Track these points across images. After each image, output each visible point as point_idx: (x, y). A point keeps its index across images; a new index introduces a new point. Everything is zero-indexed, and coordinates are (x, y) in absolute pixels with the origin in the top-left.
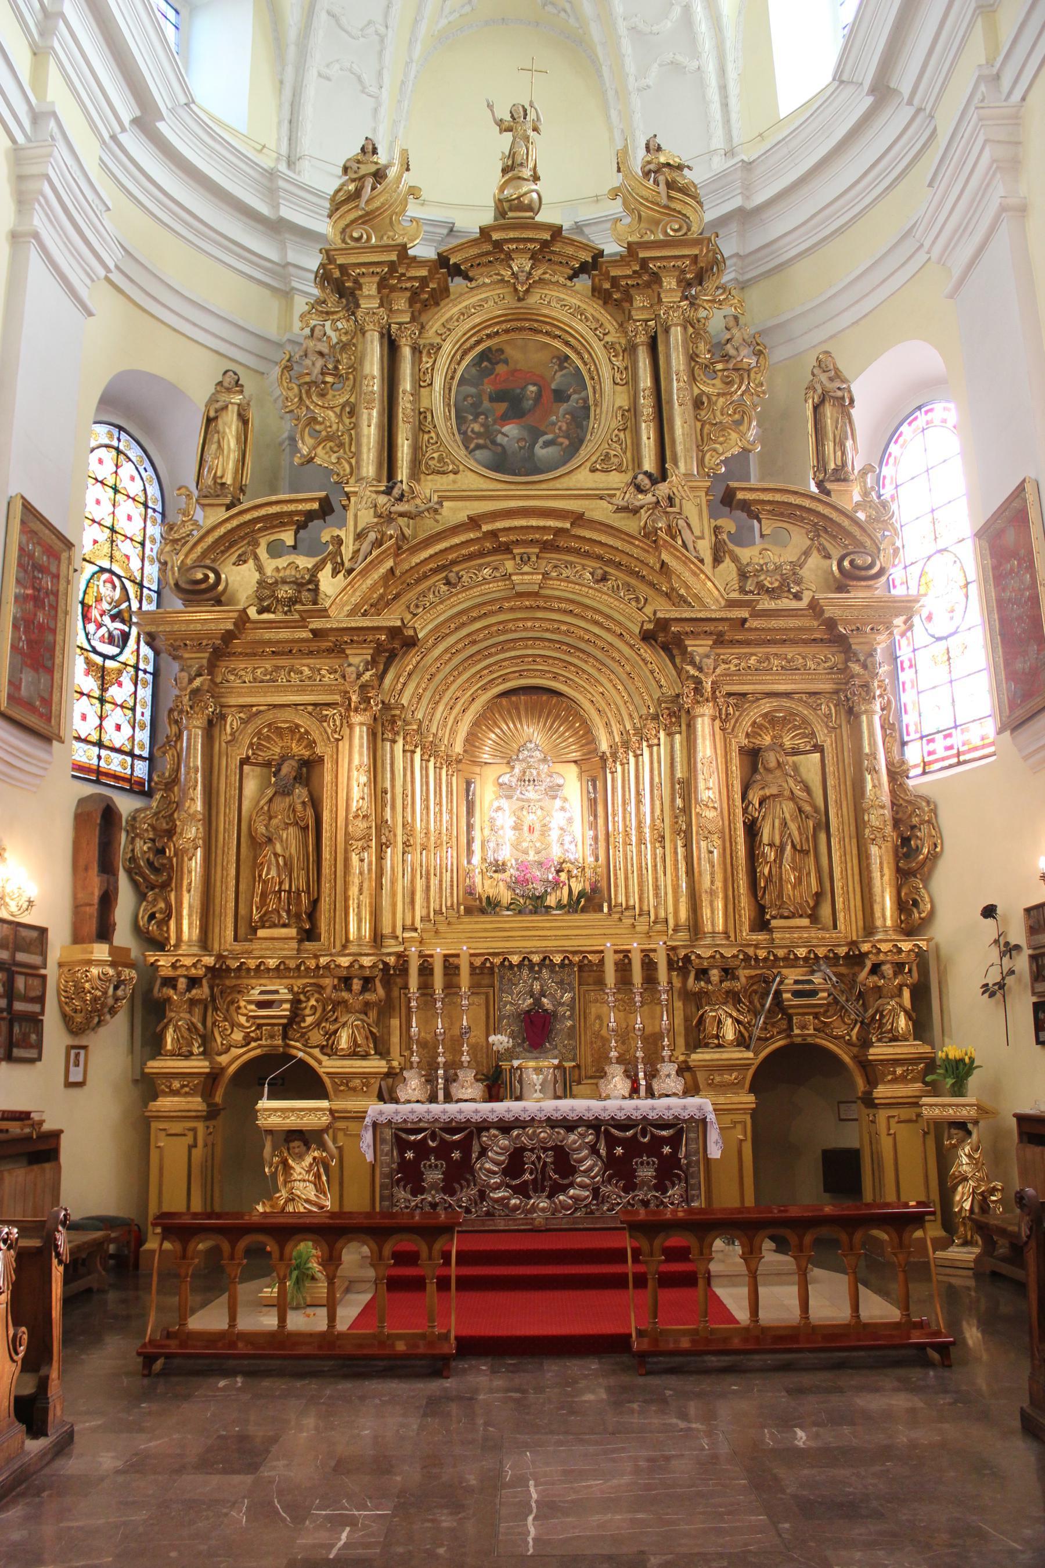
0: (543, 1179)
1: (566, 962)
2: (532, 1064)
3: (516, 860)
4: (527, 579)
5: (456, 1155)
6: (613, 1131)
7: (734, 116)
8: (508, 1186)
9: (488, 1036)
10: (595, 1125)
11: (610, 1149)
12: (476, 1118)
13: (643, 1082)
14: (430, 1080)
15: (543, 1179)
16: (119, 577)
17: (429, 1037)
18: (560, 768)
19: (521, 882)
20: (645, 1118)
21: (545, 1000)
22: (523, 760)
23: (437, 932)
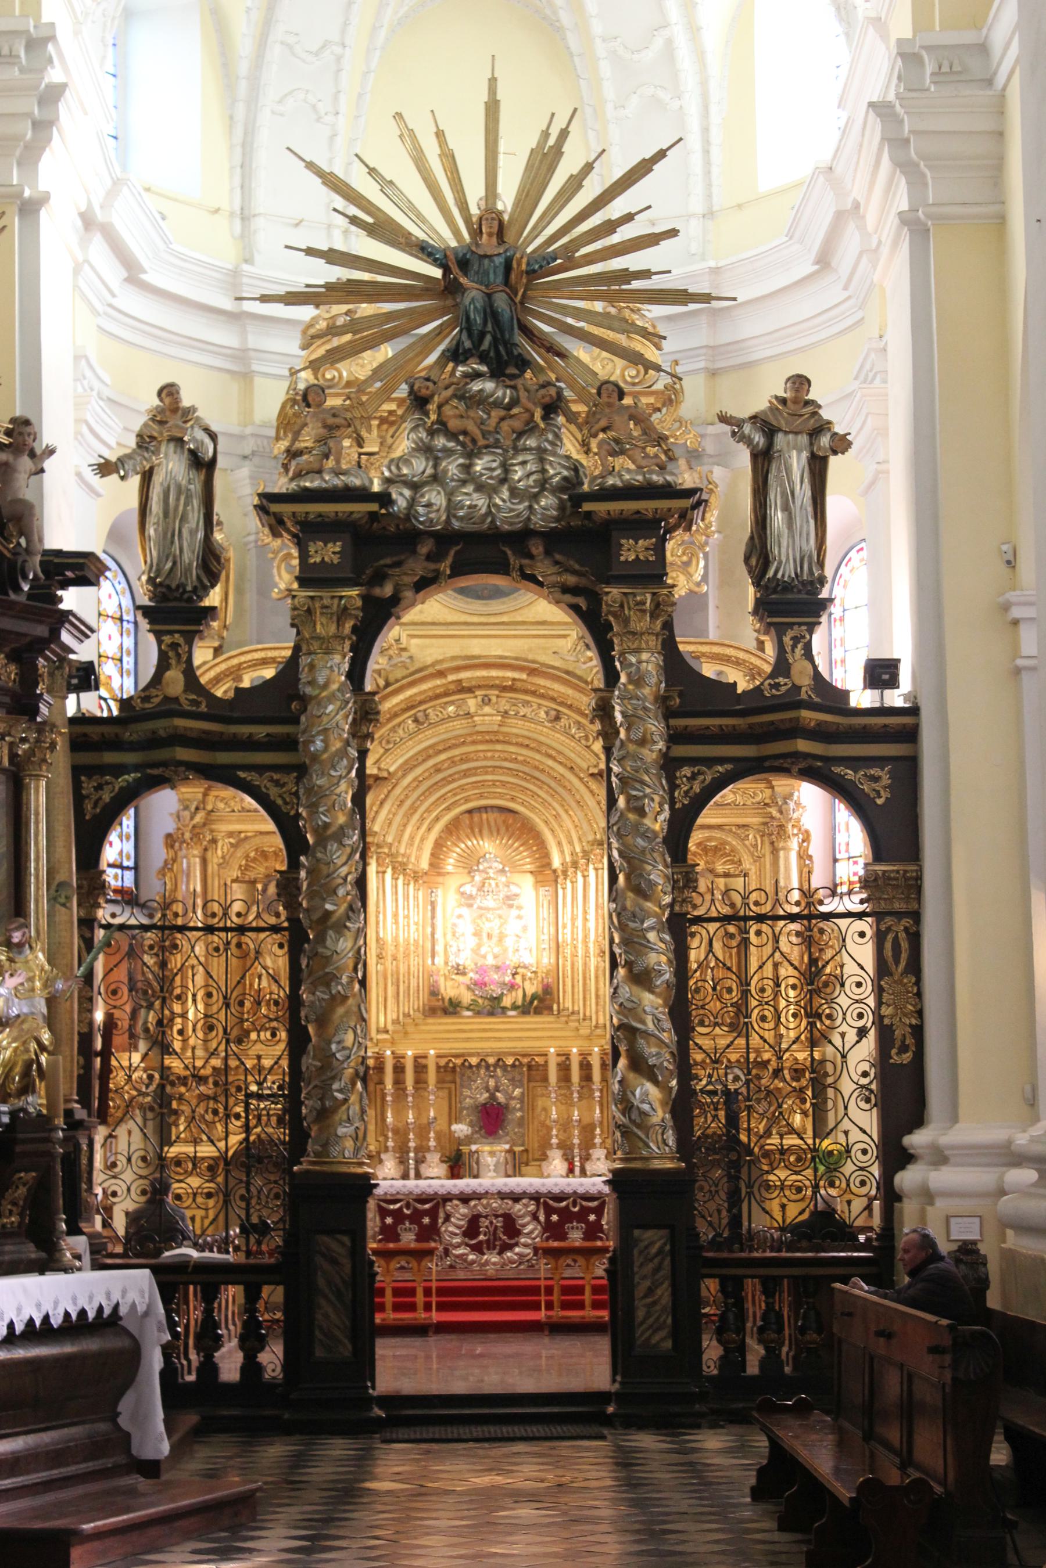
0: (495, 1239)
2: (487, 1148)
4: (488, 718)
5: (426, 1220)
6: (551, 1202)
7: (715, 170)
8: (467, 1245)
9: (450, 1124)
10: (536, 1197)
11: (548, 1216)
12: (442, 1191)
13: (577, 1164)
14: (403, 1161)
15: (495, 1239)
16: (105, 700)
17: (400, 1125)
18: (517, 878)
19: (480, 984)
20: (575, 1192)
21: (498, 1094)
23: (406, 1033)
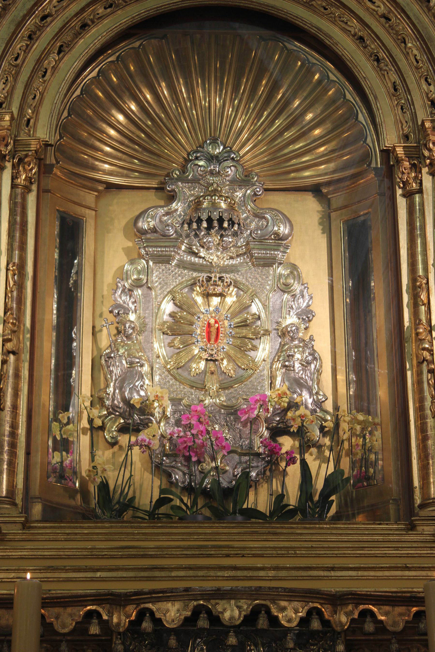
1: (316, 625)
3: (175, 401)
22: (195, 181)
